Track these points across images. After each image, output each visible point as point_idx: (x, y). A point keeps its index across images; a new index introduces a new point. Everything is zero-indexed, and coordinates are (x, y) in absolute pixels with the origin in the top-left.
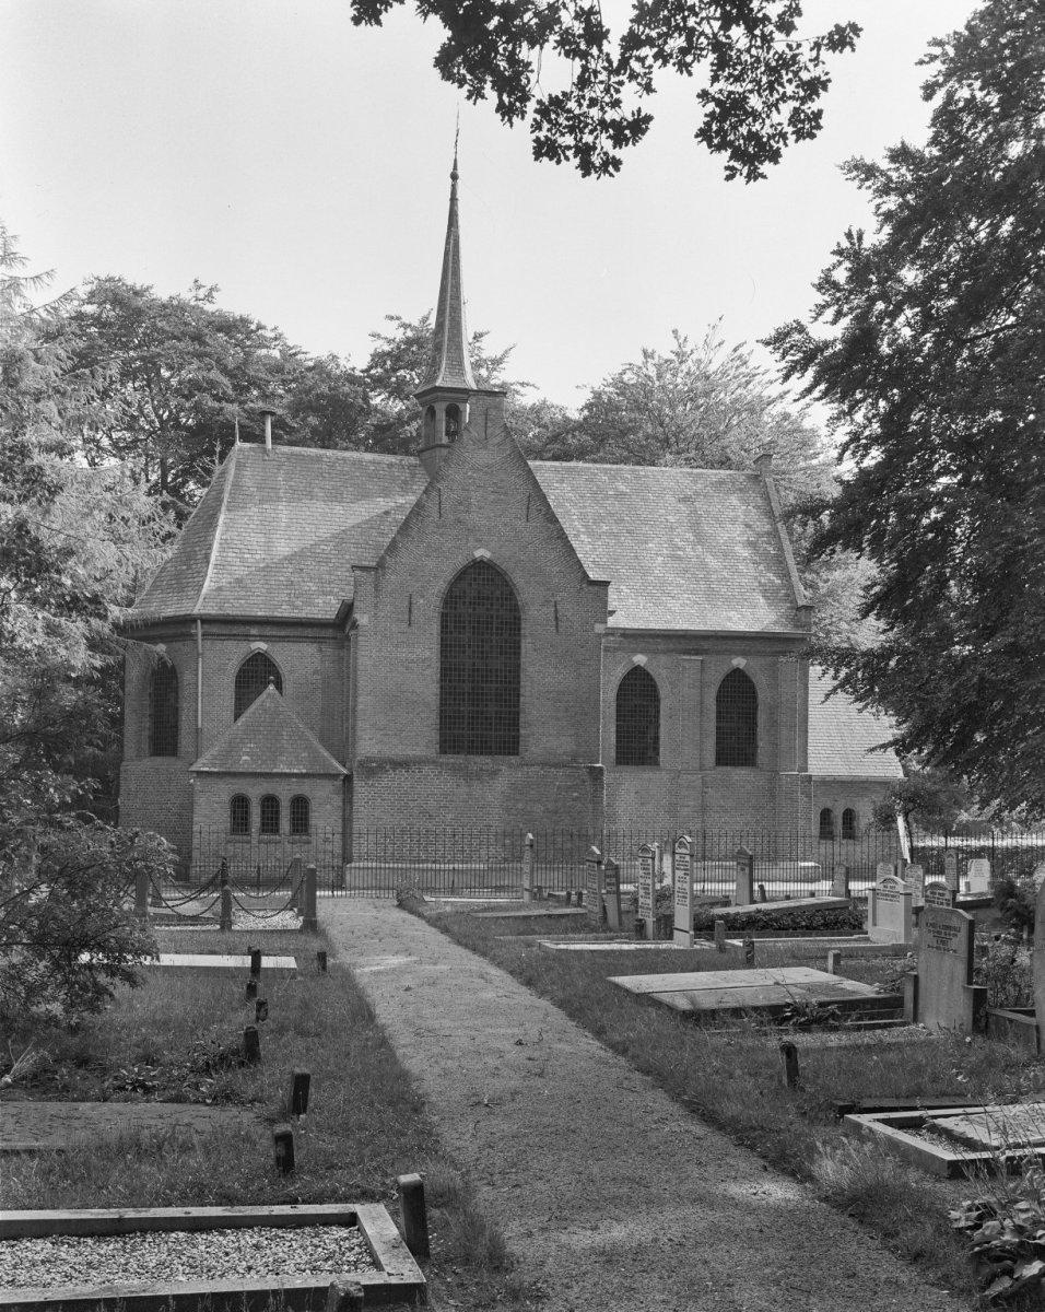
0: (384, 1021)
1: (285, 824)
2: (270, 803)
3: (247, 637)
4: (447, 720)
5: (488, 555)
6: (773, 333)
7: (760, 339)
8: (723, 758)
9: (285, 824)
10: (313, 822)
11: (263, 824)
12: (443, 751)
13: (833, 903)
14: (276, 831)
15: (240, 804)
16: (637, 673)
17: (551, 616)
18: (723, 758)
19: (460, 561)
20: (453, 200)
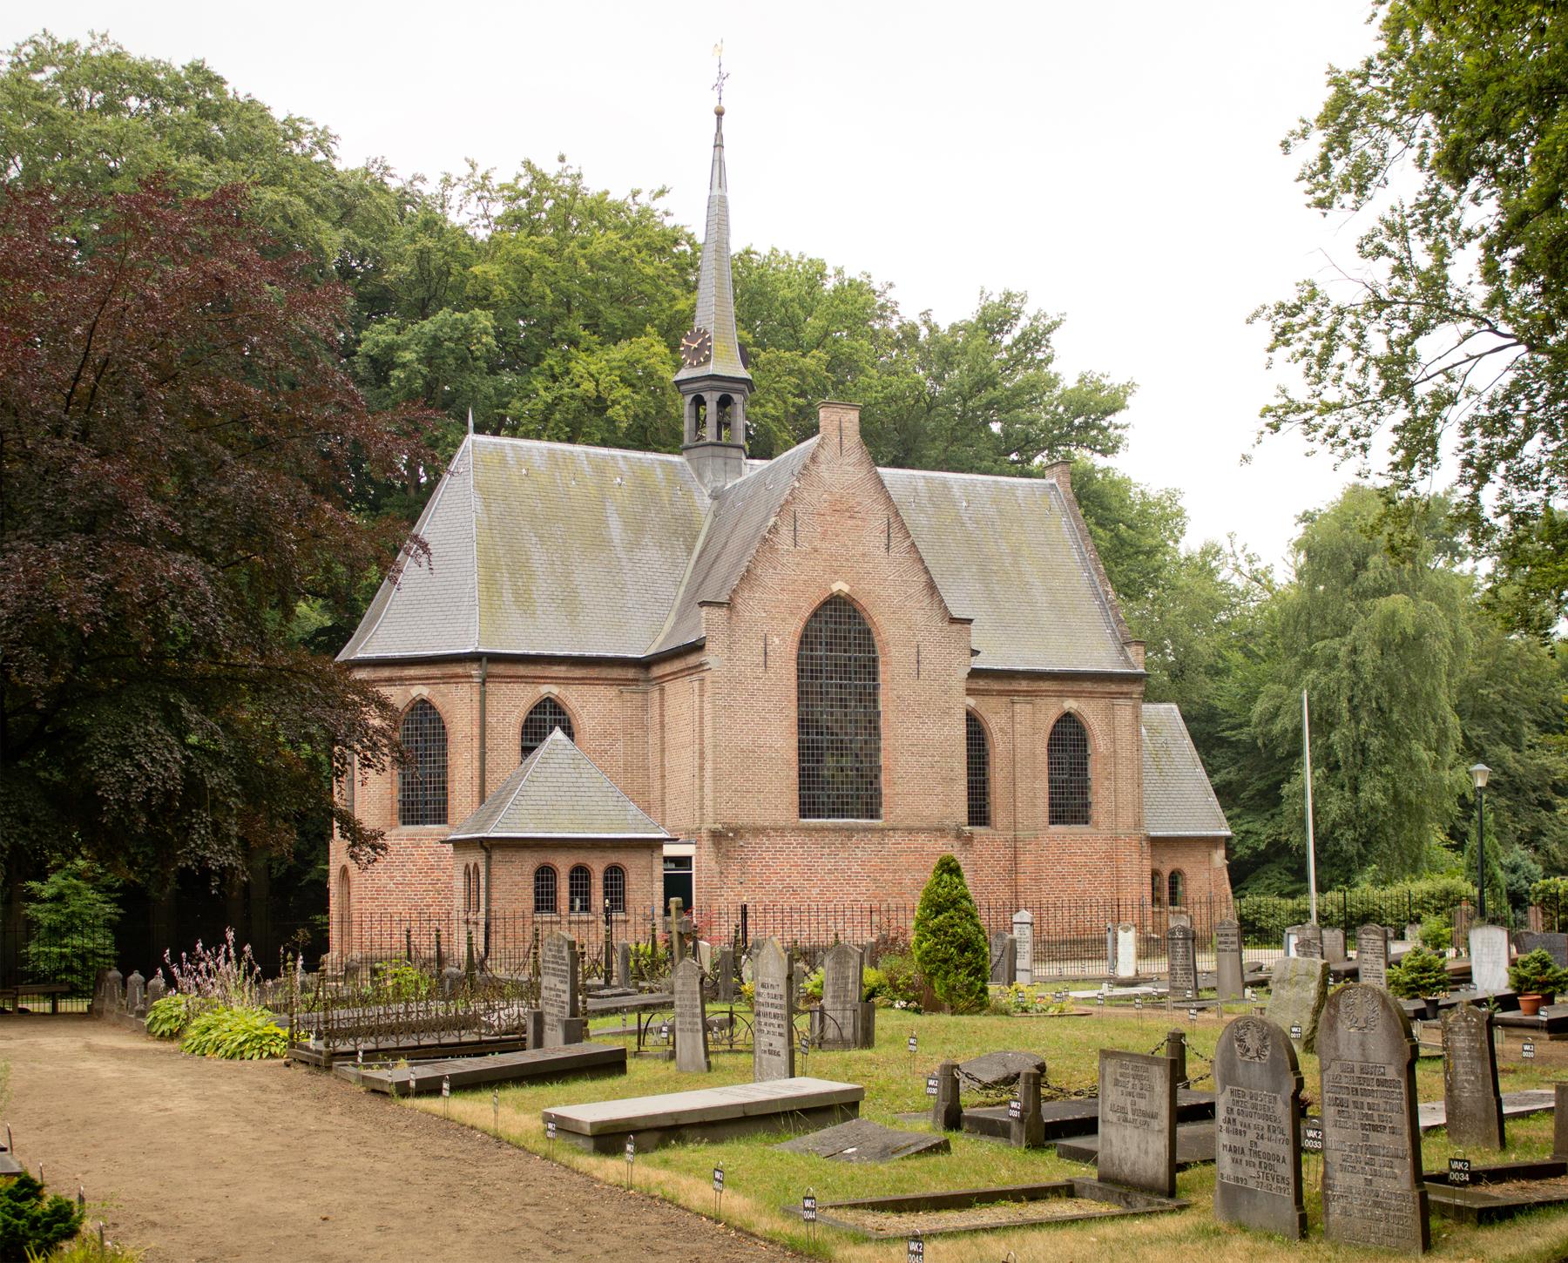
0: (66, 1250)
1: (598, 899)
2: (580, 876)
3: (1061, 695)
4: (808, 779)
5: (846, 588)
6: (180, 61)
7: (470, 158)
8: (1057, 817)
9: (598, 899)
10: (630, 896)
11: (537, 901)
12: (803, 814)
13: (568, 1103)
14: (553, 909)
15: (545, 876)
16: (1067, 718)
17: (913, 658)
18: (1057, 817)
19: (817, 597)
20: (719, 164)
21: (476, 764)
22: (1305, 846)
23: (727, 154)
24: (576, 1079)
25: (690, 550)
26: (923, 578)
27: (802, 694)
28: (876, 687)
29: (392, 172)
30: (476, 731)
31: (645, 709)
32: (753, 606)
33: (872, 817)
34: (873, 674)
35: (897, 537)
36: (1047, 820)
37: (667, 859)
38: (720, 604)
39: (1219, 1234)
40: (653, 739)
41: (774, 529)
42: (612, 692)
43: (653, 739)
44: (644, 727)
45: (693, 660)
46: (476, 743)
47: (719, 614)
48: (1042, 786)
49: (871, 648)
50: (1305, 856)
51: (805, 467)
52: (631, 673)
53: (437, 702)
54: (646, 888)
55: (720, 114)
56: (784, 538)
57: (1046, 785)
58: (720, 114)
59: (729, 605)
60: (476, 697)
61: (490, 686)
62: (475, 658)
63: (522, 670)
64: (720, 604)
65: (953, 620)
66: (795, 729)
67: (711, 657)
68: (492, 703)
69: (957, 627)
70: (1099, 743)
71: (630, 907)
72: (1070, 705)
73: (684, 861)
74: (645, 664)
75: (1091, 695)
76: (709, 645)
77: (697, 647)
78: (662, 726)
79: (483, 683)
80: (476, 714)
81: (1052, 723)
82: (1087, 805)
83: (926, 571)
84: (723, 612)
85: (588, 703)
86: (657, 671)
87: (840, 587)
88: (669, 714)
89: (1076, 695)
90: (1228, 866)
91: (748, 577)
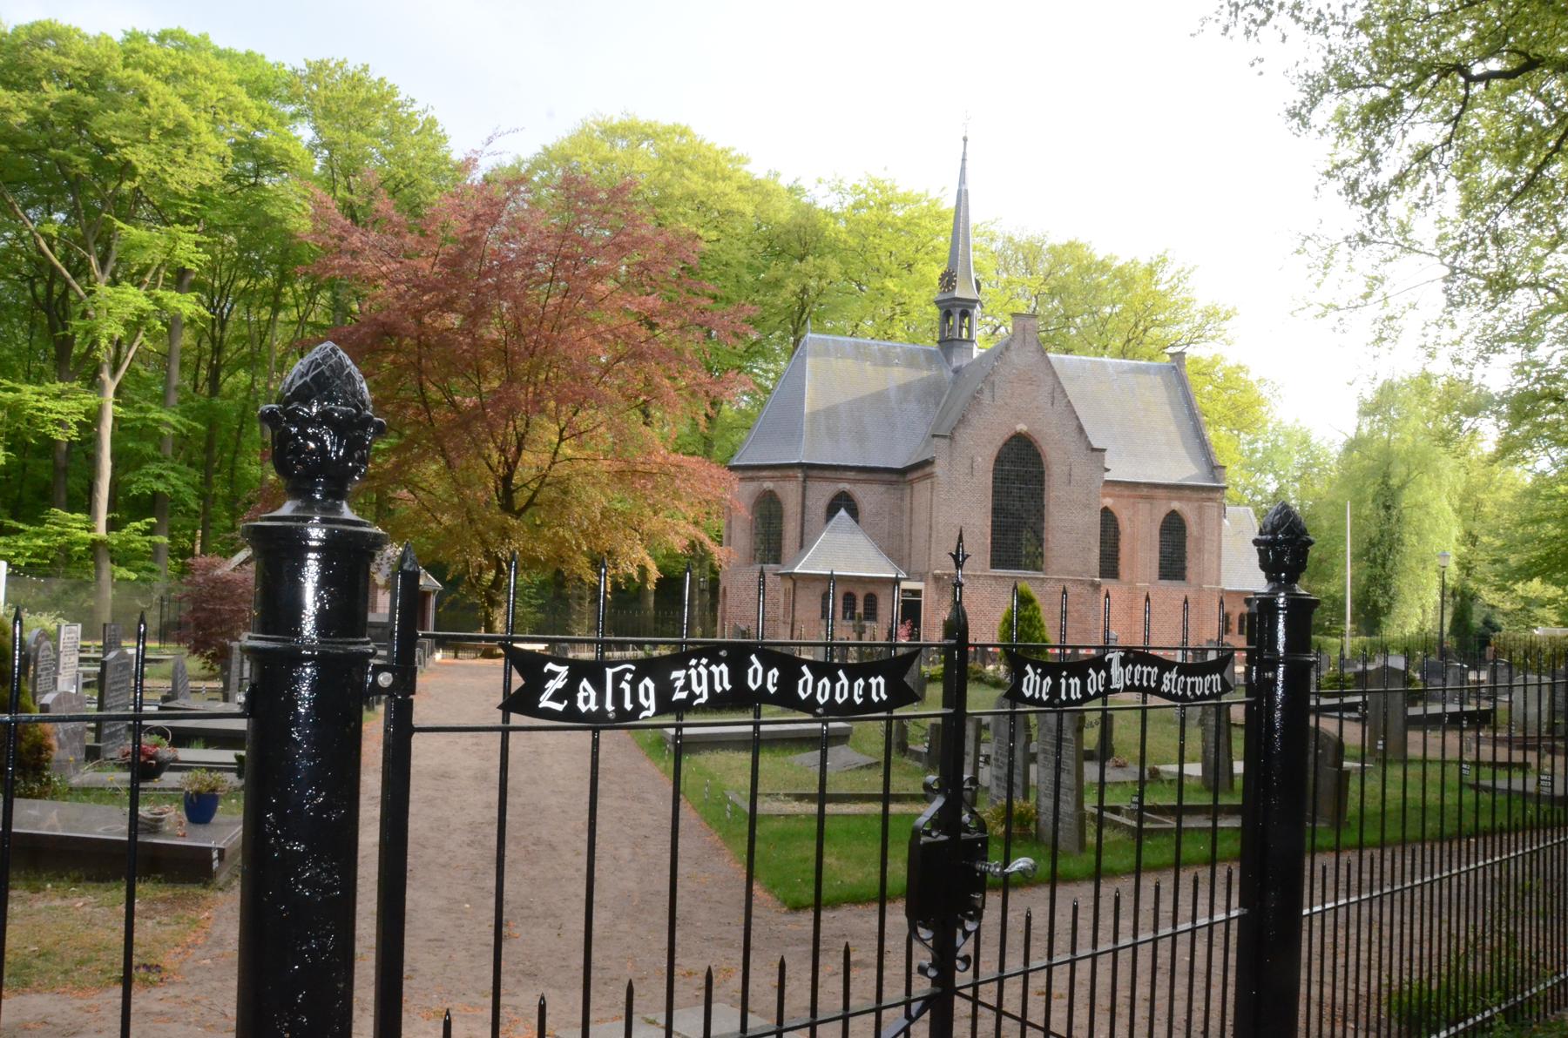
20: (963, 169)
21: (799, 529)
22: (1344, 598)
23: (968, 164)
24: (723, 750)
25: (937, 404)
26: (1075, 423)
27: (996, 492)
28: (1043, 490)
29: (733, 154)
30: (799, 509)
31: (902, 499)
32: (965, 437)
33: (1037, 570)
34: (1041, 482)
35: (1058, 395)
36: (1156, 576)
37: (904, 591)
38: (944, 437)
39: (1325, 268)
40: (906, 518)
41: (980, 391)
42: (882, 488)
43: (906, 518)
44: (902, 512)
45: (928, 470)
46: (799, 516)
47: (944, 443)
48: (1155, 556)
49: (1040, 464)
50: (1344, 605)
51: (1001, 353)
52: (894, 477)
53: (778, 492)
54: (889, 608)
55: (965, 140)
56: (986, 398)
57: (1158, 555)
58: (965, 140)
59: (951, 438)
60: (800, 490)
61: (809, 484)
62: (800, 466)
63: (827, 474)
64: (944, 437)
65: (1094, 450)
66: (990, 514)
67: (939, 469)
68: (809, 493)
69: (1095, 453)
70: (1192, 529)
71: (879, 618)
72: (1176, 505)
73: (917, 593)
74: (903, 472)
75: (1189, 500)
76: (937, 461)
77: (928, 463)
78: (911, 510)
79: (804, 481)
80: (800, 499)
81: (1163, 516)
82: (1184, 569)
83: (1077, 418)
84: (947, 441)
85: (868, 496)
86: (910, 477)
87: (1022, 427)
88: (915, 503)
89: (1179, 499)
90: (413, 693)
91: (963, 420)
